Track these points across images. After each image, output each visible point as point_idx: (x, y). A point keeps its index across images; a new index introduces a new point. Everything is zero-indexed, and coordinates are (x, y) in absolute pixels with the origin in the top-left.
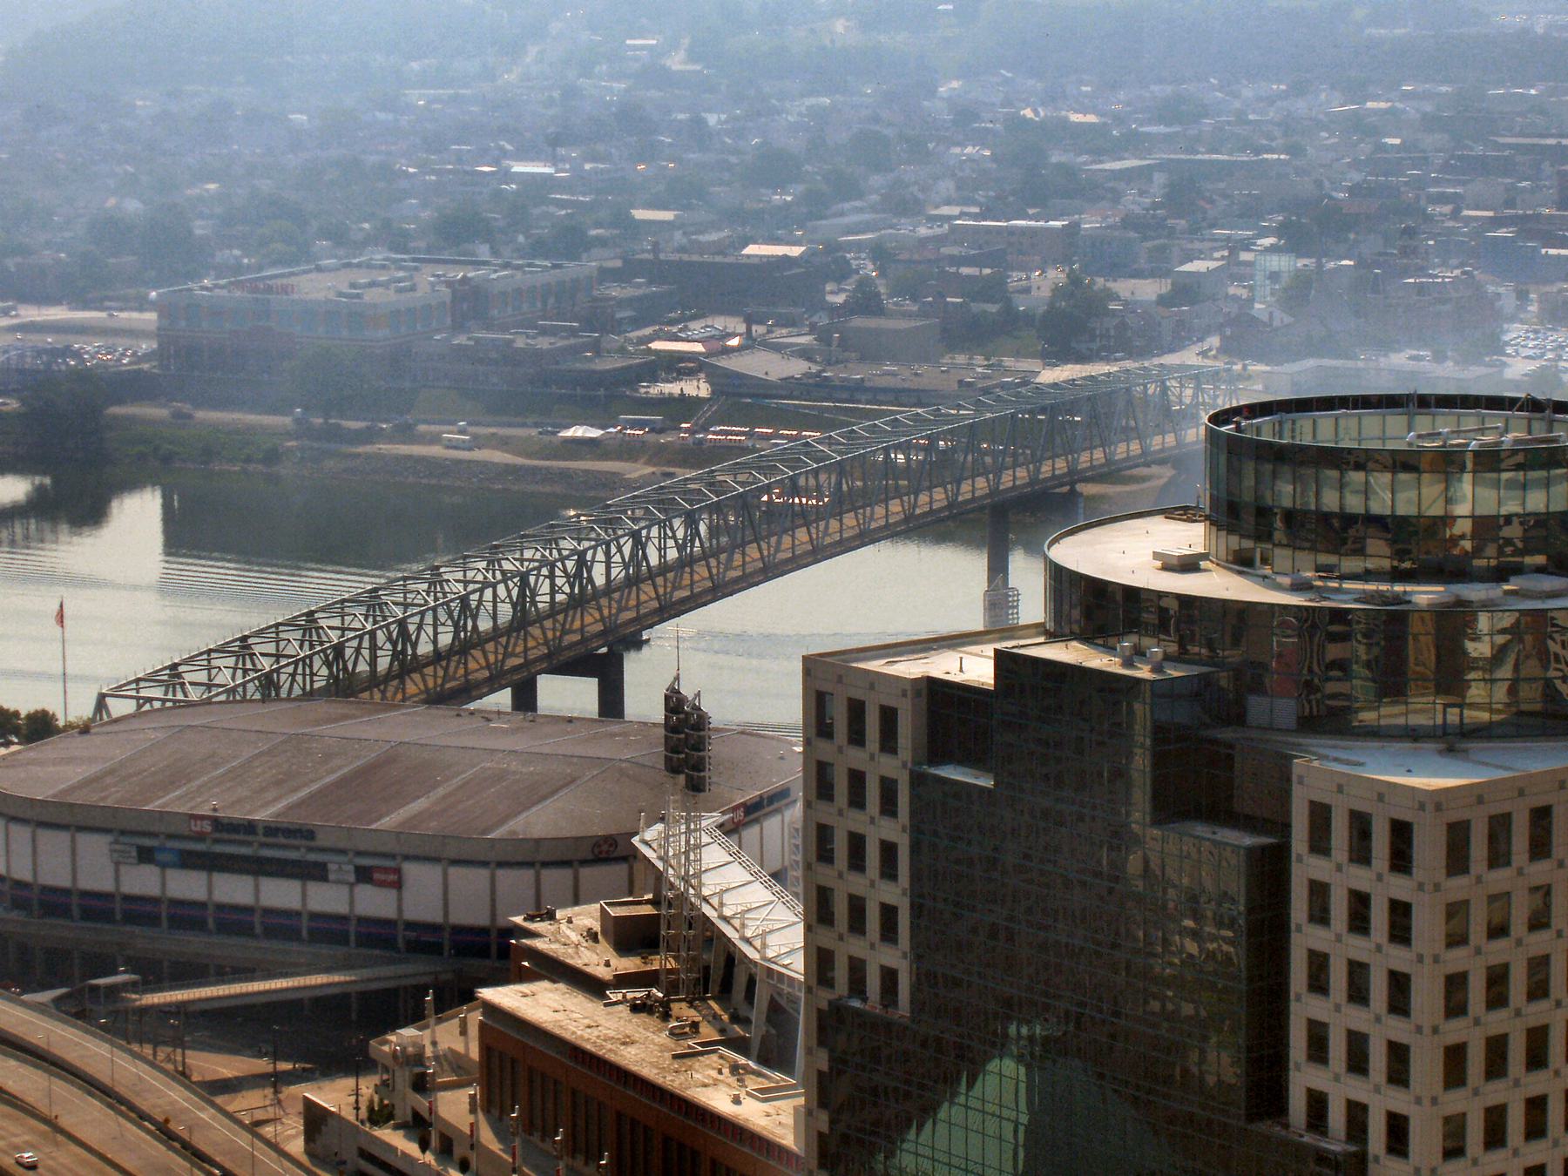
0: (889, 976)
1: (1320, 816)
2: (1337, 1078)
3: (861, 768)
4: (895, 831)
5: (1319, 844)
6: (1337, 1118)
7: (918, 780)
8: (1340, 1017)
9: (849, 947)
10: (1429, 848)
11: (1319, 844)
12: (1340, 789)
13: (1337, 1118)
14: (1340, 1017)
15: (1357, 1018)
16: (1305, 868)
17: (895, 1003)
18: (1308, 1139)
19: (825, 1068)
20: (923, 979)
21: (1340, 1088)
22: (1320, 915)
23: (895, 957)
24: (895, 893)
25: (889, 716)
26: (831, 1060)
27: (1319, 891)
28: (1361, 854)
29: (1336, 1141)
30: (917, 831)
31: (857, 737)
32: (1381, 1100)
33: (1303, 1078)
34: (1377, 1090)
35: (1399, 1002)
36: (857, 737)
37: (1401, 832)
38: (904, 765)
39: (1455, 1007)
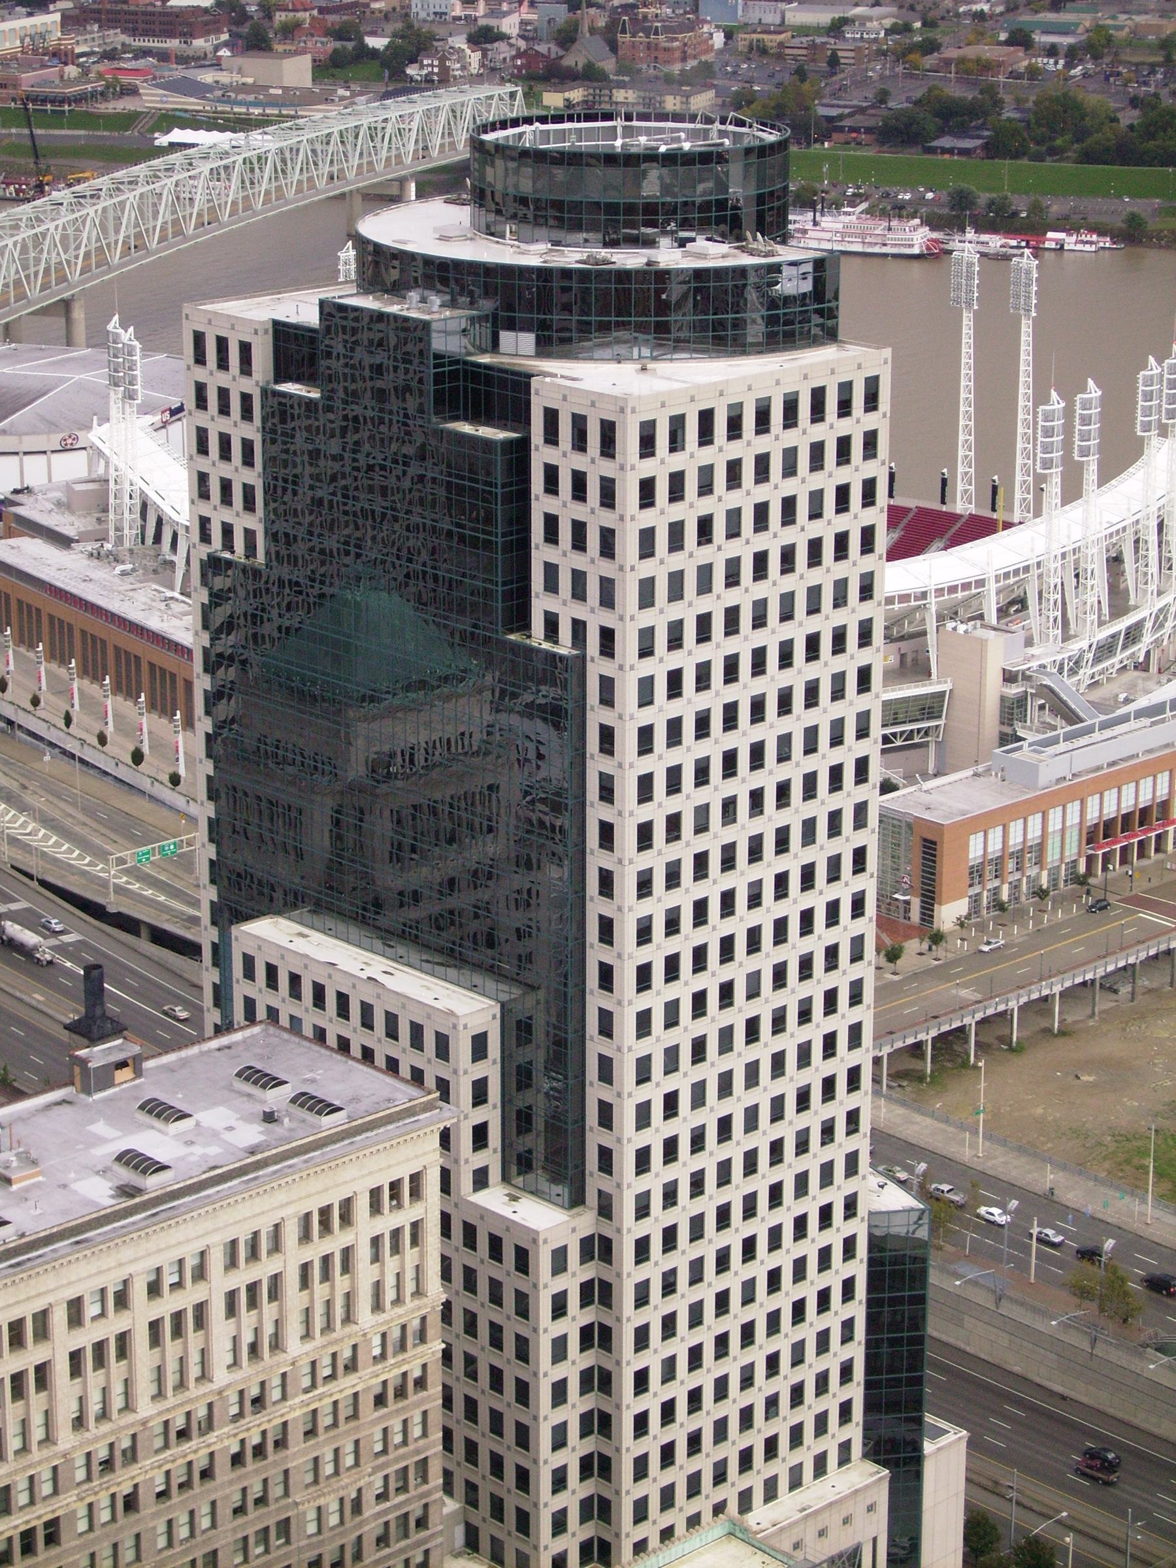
0: (249, 534)
1: (551, 417)
2: (565, 603)
3: (228, 476)
4: (252, 431)
5: (551, 437)
6: (565, 632)
7: (265, 392)
8: (566, 460)
9: (219, 516)
10: (628, 440)
11: (551, 437)
12: (565, 398)
13: (565, 632)
14: (566, 460)
15: (579, 511)
16: (541, 455)
17: (255, 556)
18: (546, 646)
19: (215, 899)
20: (272, 536)
21: (567, 610)
22: (551, 585)
23: (255, 522)
24: (253, 477)
25: (245, 348)
26: (210, 595)
27: (551, 571)
28: (580, 443)
29: (564, 647)
30: (268, 523)
31: (223, 364)
32: (596, 619)
33: (540, 604)
34: (592, 611)
35: (608, 600)
36: (223, 364)
37: (608, 432)
38: (257, 384)
39: (646, 699)
